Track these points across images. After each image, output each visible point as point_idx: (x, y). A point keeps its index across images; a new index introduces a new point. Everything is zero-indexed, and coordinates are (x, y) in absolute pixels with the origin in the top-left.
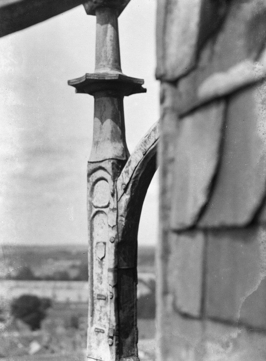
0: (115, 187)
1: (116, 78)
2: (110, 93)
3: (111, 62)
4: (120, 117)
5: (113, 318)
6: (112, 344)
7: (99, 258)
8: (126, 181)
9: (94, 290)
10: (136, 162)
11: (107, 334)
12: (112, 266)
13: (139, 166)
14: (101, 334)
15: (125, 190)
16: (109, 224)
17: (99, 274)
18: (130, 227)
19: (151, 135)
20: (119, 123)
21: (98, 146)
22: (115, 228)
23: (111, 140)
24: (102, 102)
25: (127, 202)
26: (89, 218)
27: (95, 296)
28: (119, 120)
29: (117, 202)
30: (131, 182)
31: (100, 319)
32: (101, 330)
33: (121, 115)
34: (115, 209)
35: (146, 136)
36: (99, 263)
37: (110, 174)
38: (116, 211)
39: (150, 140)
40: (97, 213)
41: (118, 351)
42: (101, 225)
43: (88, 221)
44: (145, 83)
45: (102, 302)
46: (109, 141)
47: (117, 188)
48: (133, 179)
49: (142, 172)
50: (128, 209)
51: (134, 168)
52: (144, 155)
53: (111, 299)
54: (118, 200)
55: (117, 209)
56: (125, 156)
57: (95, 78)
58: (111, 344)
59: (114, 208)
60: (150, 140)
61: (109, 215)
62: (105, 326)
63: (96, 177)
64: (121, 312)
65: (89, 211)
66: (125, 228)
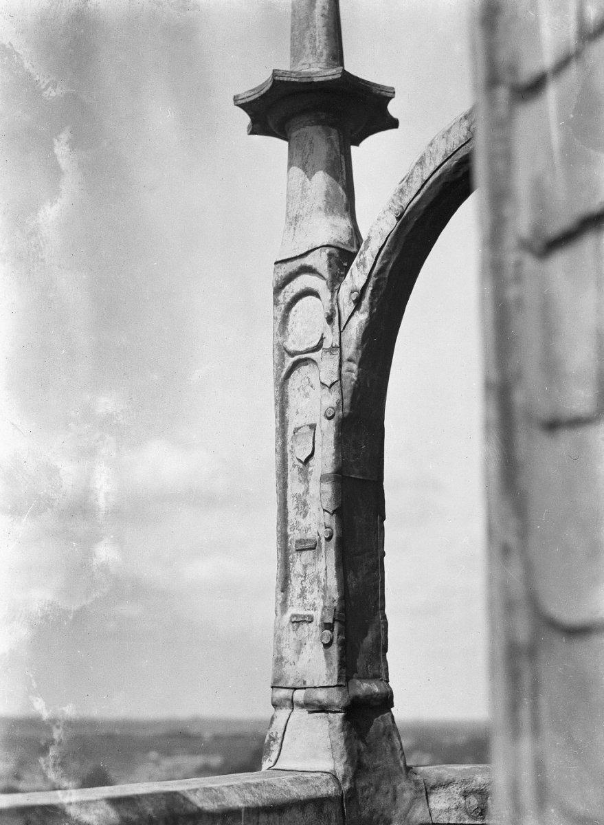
0: (335, 301)
1: (335, 77)
2: (323, 117)
3: (324, 57)
4: (344, 166)
5: (333, 583)
6: (332, 641)
7: (300, 461)
8: (360, 283)
9: (289, 532)
11: (319, 623)
12: (329, 470)
14: (305, 625)
15: (358, 303)
16: (323, 381)
17: (300, 496)
18: (368, 386)
20: (342, 178)
22: (336, 388)
23: (325, 210)
24: (306, 135)
25: (361, 329)
26: (277, 380)
27: (292, 546)
29: (341, 332)
30: (371, 283)
31: (302, 594)
32: (305, 616)
34: (336, 347)
36: (301, 471)
37: (324, 279)
38: (338, 352)
40: (296, 365)
41: (344, 659)
42: (304, 390)
43: (276, 386)
45: (307, 555)
46: (321, 214)
47: (340, 303)
48: (375, 276)
50: (365, 345)
52: (398, 219)
53: (328, 539)
54: (342, 329)
55: (340, 347)
56: (355, 245)
57: (293, 80)
58: (326, 641)
59: (332, 347)
60: (411, 185)
61: (321, 364)
62: (314, 607)
63: (292, 292)
64: (351, 575)
65: (278, 365)
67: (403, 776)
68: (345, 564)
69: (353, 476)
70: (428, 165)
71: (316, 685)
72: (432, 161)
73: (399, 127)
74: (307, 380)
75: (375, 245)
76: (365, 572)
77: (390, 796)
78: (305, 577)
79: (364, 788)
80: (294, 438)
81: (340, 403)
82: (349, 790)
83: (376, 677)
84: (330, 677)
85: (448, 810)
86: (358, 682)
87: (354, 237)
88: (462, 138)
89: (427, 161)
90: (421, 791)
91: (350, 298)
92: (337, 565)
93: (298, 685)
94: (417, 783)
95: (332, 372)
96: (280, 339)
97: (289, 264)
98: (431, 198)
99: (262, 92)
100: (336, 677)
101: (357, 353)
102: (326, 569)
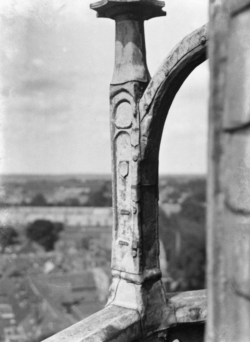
0: (137, 108)
2: (131, 16)
4: (141, 40)
5: (137, 231)
8: (149, 102)
9: (118, 205)
10: (158, 84)
11: (131, 247)
12: (135, 184)
13: (161, 87)
15: (148, 111)
16: (132, 144)
19: (174, 56)
20: (140, 46)
21: (121, 68)
22: (138, 148)
23: (133, 63)
25: (149, 122)
26: (112, 138)
27: (119, 212)
28: (140, 43)
29: (140, 122)
30: (153, 106)
31: (124, 232)
33: (142, 39)
34: (138, 129)
35: (168, 58)
36: (123, 180)
38: (139, 131)
39: (172, 61)
40: (120, 133)
43: (111, 141)
44: (166, 5)
45: (126, 217)
46: (131, 64)
47: (140, 109)
48: (156, 100)
49: (164, 92)
51: (157, 89)
52: (166, 76)
53: (135, 213)
54: (140, 121)
55: (140, 129)
56: (146, 78)
58: (134, 255)
60: (172, 61)
61: (132, 135)
63: (118, 99)
64: (144, 226)
65: (112, 132)
66: (147, 147)
67: (165, 305)
68: (141, 222)
69: (145, 185)
70: (180, 53)
71: (130, 272)
72: (182, 51)
73: (164, 1)
74: (125, 141)
75: (156, 86)
76: (150, 224)
77: (160, 315)
78: (125, 226)
79: (150, 313)
80: (120, 165)
81: (140, 154)
82: (144, 316)
83: (155, 267)
84: (136, 270)
85: (184, 317)
86: (147, 271)
87: (146, 74)
88: (196, 43)
89: (180, 51)
90: (173, 311)
91: (144, 108)
92: (139, 224)
93: (123, 270)
94: (171, 308)
95: (136, 140)
96: (113, 120)
97: (117, 86)
98: (181, 68)
99: (103, 5)
100: (138, 270)
101: (147, 133)
102: (134, 225)
